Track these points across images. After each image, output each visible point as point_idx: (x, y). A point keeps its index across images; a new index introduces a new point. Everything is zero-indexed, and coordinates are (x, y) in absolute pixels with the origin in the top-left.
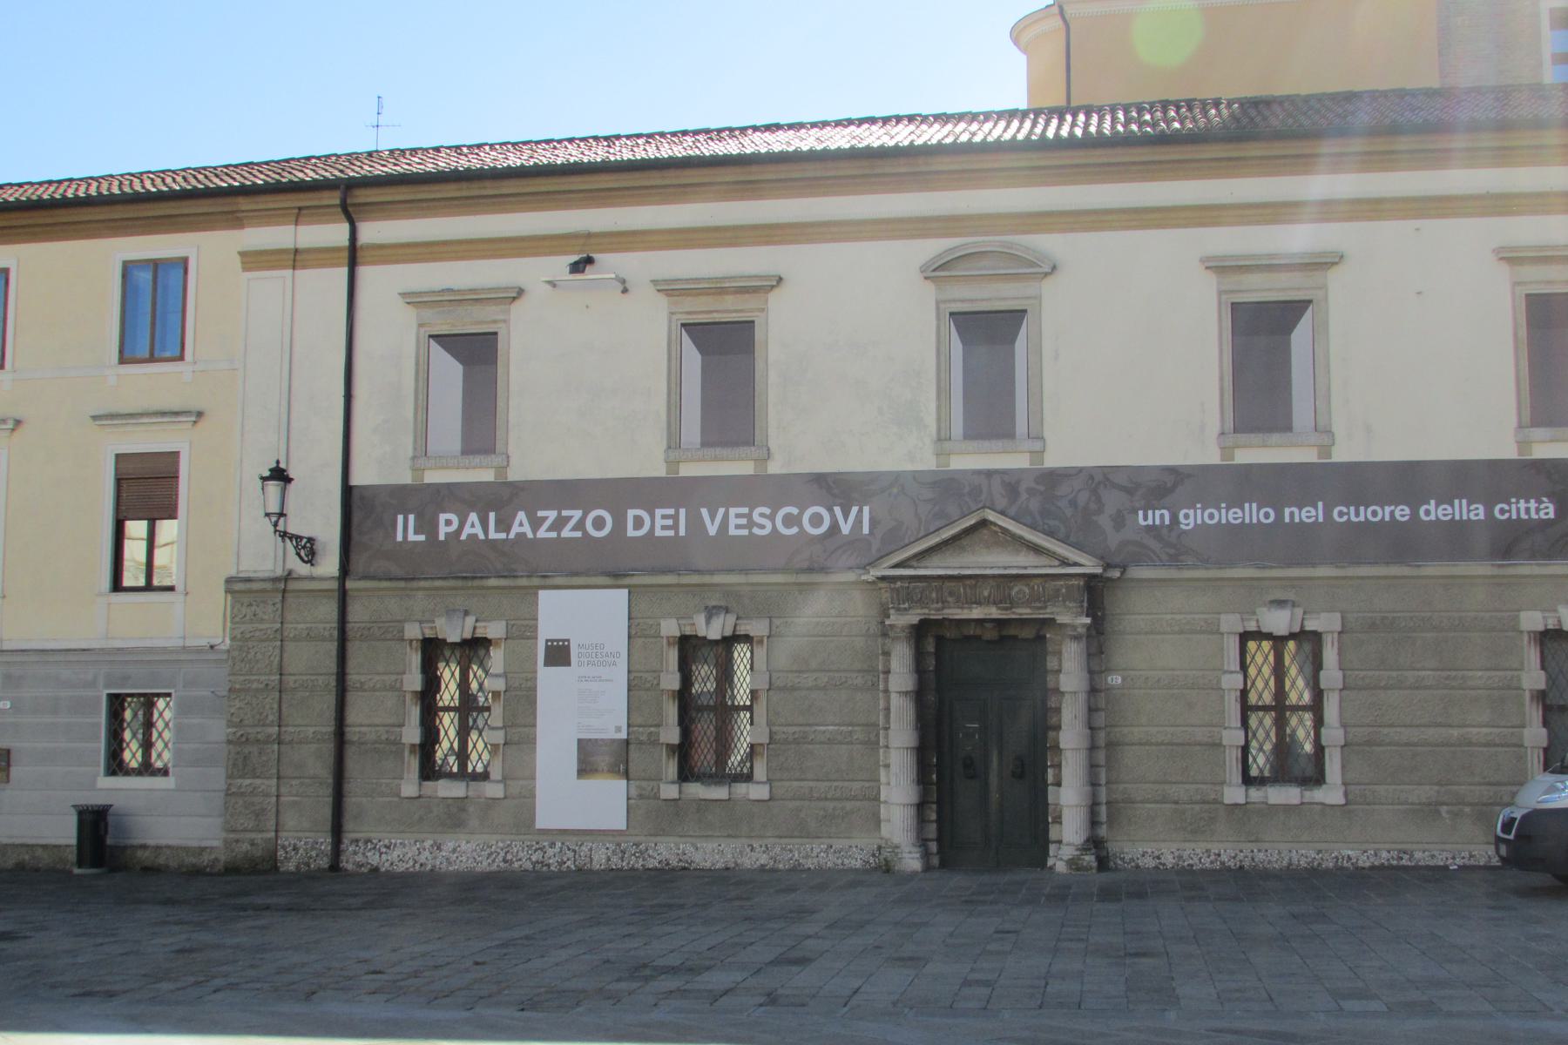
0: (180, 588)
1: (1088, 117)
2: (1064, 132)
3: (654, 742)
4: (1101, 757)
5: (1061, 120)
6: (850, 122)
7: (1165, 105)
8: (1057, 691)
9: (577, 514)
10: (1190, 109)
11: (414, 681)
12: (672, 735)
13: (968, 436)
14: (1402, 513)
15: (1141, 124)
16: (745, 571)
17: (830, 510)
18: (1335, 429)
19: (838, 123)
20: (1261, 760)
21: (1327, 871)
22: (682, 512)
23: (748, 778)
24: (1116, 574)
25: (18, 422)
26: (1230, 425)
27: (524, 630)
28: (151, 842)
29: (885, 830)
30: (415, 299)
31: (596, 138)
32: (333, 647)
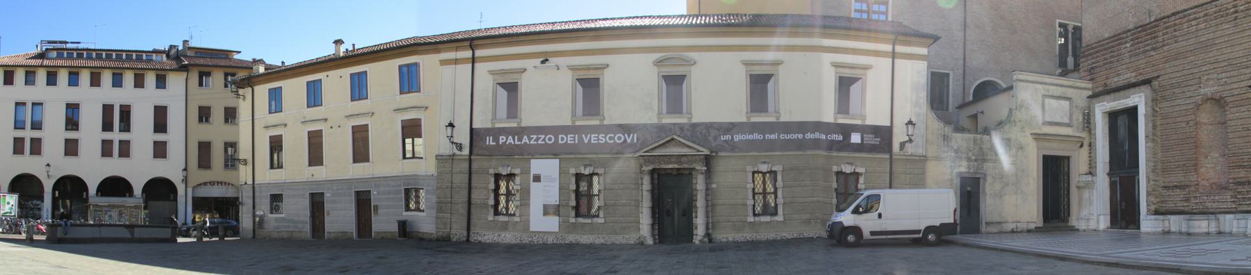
0: (424, 158)
1: (706, 18)
2: (698, 22)
3: (567, 205)
4: (710, 209)
5: (697, 18)
6: (630, 18)
7: (729, 15)
8: (696, 189)
9: (543, 136)
10: (737, 16)
11: (492, 186)
12: (573, 203)
13: (667, 113)
14: (800, 136)
15: (722, 20)
16: (596, 154)
17: (624, 135)
18: (781, 112)
19: (626, 18)
20: (759, 209)
21: (779, 241)
22: (577, 136)
23: (598, 216)
24: (714, 154)
25: (373, 113)
26: (749, 110)
27: (526, 171)
28: (421, 231)
29: (641, 232)
30: (492, 73)
31: (549, 23)
32: (467, 175)
